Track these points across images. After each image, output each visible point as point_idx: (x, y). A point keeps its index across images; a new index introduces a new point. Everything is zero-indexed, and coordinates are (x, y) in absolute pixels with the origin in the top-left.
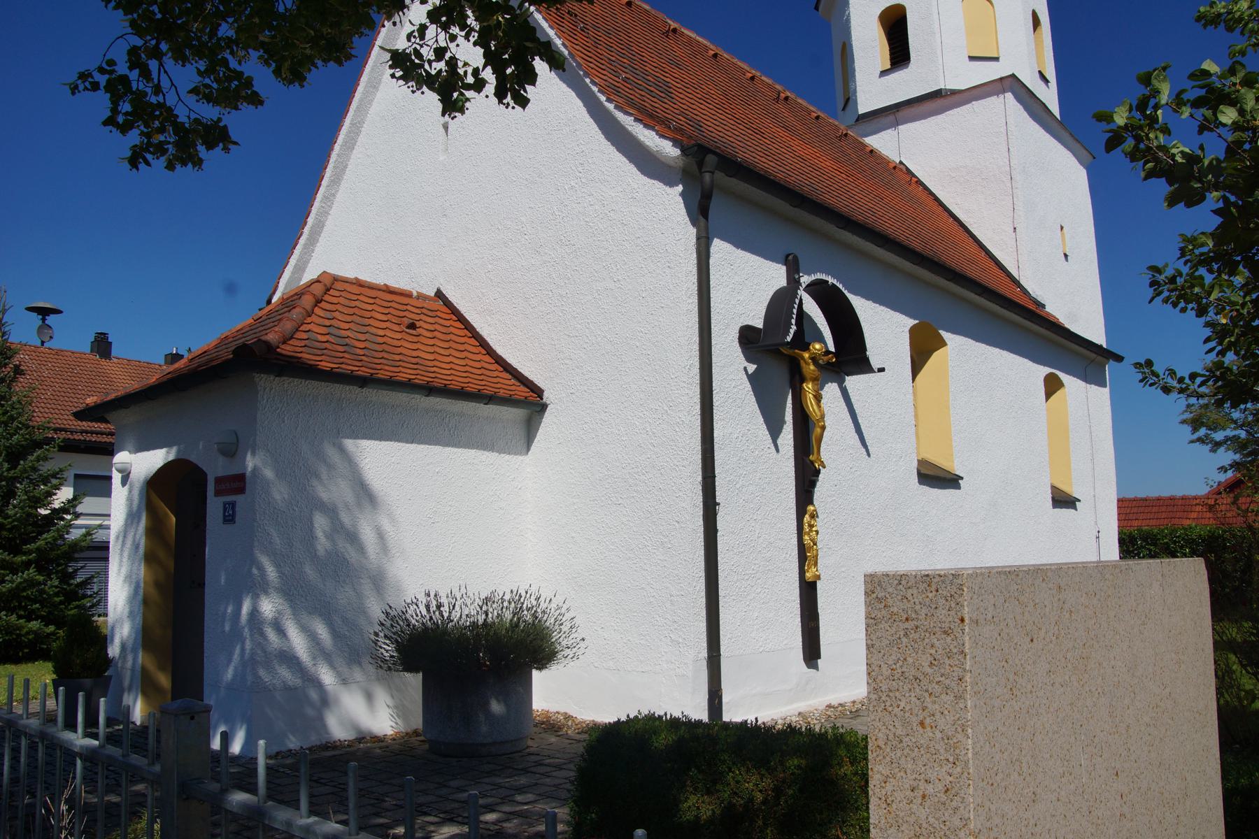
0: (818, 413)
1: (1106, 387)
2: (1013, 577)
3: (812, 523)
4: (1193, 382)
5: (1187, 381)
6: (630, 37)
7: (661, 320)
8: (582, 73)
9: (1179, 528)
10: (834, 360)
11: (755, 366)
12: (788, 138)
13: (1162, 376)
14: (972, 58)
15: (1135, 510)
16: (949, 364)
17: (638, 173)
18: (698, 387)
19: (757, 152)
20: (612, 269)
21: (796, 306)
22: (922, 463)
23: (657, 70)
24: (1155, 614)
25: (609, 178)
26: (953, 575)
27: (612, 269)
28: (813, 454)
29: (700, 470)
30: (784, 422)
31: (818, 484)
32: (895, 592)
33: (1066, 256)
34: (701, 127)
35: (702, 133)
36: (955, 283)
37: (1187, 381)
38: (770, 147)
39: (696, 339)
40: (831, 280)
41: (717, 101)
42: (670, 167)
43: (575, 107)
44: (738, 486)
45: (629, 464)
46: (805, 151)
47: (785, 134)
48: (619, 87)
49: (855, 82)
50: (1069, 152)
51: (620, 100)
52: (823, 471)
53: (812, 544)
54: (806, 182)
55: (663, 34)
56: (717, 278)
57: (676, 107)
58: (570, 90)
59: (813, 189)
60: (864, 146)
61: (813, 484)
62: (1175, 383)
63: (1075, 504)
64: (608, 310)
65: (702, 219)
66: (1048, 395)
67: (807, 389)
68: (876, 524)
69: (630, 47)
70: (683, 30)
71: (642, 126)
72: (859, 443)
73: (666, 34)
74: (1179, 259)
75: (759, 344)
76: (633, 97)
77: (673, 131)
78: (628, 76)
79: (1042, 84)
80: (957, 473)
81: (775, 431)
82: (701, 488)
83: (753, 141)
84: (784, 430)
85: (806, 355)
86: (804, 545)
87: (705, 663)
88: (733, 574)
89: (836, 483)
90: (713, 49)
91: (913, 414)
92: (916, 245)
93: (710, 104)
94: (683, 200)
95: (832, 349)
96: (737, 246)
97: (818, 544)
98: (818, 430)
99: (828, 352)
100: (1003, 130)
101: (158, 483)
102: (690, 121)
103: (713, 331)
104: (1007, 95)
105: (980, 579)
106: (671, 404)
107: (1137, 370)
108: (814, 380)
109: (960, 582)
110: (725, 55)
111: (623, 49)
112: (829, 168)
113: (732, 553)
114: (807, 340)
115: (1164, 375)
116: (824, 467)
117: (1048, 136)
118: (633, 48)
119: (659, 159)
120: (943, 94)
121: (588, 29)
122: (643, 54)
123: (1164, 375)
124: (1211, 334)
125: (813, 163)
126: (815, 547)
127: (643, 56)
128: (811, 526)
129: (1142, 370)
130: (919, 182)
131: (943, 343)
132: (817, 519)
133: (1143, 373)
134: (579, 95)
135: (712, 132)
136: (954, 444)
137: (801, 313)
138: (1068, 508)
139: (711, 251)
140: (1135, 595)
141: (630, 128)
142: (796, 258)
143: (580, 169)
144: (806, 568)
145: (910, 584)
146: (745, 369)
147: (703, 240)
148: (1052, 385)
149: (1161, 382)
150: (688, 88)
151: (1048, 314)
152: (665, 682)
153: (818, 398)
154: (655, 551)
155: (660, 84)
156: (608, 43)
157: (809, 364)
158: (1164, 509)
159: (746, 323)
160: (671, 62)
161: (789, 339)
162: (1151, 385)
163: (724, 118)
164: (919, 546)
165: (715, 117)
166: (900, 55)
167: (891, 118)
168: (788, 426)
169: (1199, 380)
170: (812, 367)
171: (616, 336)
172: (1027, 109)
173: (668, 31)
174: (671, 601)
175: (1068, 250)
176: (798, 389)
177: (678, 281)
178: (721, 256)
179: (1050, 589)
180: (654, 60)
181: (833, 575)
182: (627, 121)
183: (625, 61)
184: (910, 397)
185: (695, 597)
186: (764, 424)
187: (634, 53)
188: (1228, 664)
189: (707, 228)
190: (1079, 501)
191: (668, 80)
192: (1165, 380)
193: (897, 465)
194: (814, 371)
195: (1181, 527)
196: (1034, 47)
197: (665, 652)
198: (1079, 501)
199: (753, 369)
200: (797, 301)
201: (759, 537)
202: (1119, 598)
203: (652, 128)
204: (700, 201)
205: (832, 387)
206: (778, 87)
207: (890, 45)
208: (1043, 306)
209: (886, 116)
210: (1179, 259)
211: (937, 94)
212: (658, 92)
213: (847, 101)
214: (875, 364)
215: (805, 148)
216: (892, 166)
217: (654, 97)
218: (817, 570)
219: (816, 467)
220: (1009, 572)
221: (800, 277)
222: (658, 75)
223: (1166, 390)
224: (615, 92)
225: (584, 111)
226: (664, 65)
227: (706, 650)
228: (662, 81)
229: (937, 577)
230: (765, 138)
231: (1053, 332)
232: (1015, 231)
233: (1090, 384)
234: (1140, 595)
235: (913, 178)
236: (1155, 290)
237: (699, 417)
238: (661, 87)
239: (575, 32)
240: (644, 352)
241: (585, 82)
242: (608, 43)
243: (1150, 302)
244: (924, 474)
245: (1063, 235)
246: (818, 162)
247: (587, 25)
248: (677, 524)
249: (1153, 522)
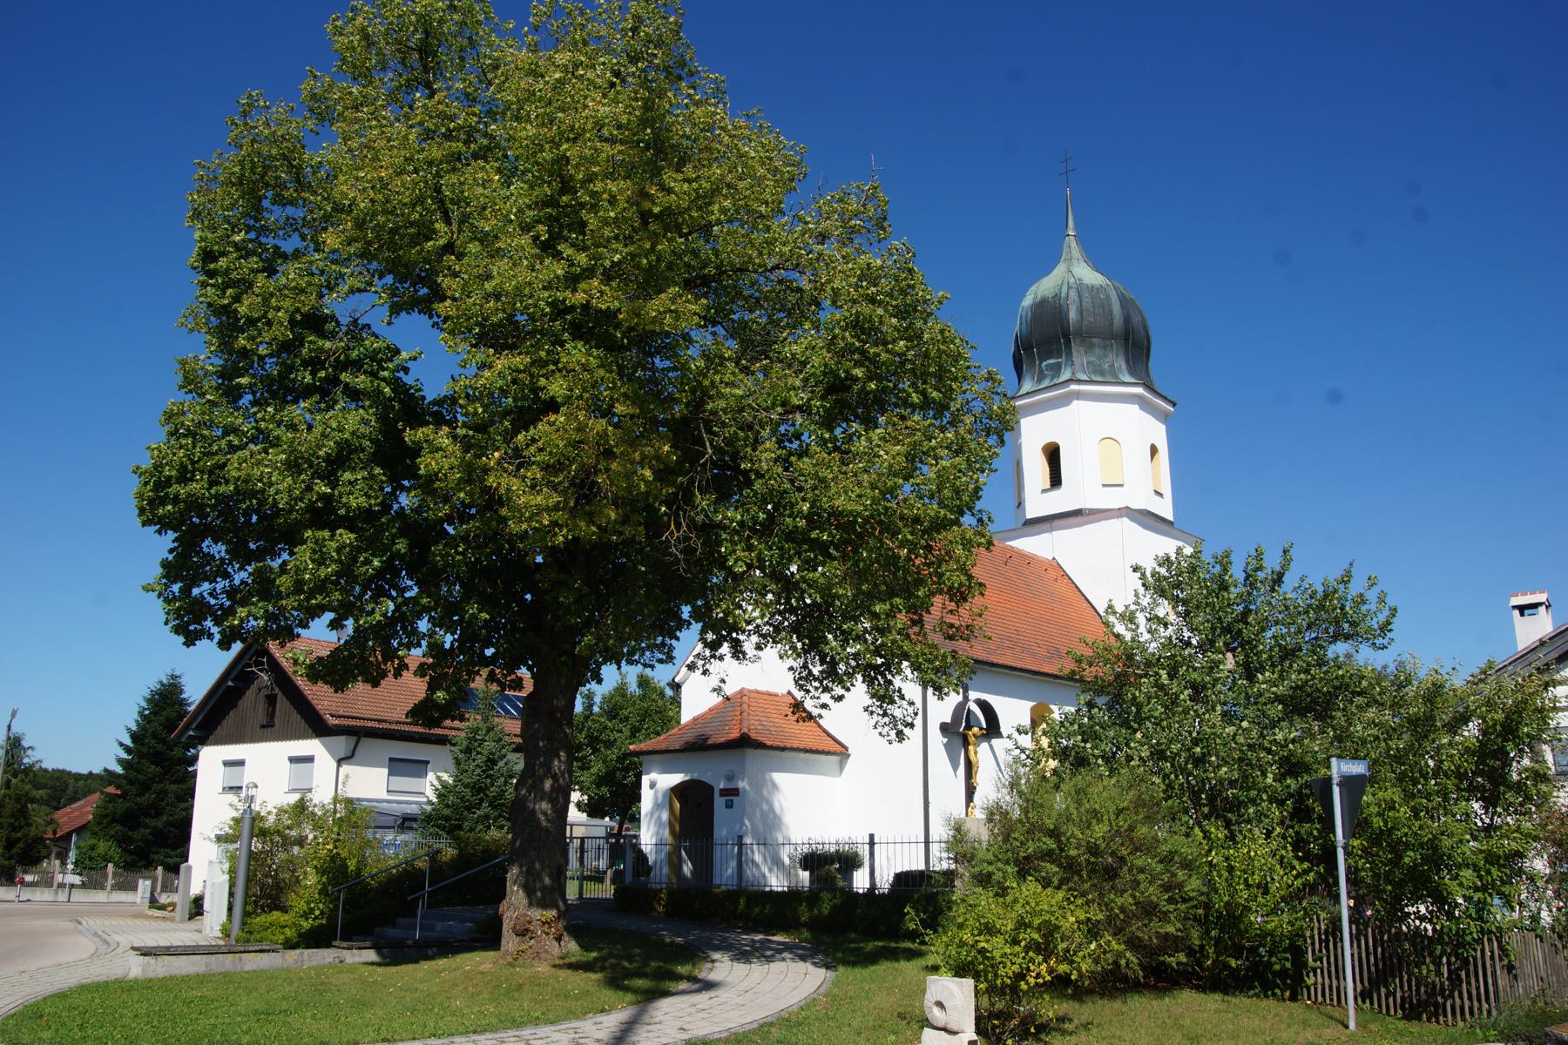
14: (1104, 485)
81: (955, 767)
101: (678, 791)
153: (976, 753)
166: (1056, 480)
167: (1047, 526)
211: (1077, 513)
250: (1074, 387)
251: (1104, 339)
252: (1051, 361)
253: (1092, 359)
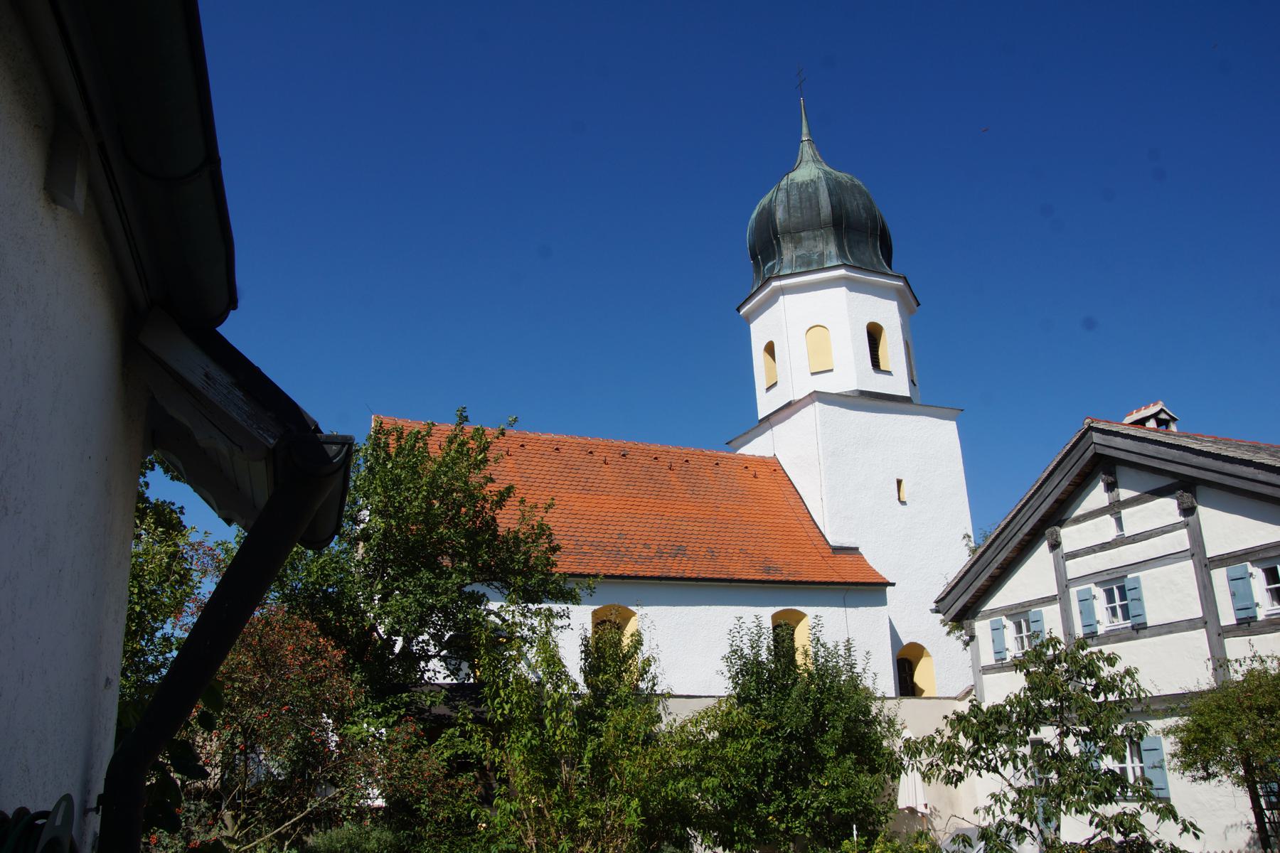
14: (813, 374)
211: (789, 404)
250: (775, 284)
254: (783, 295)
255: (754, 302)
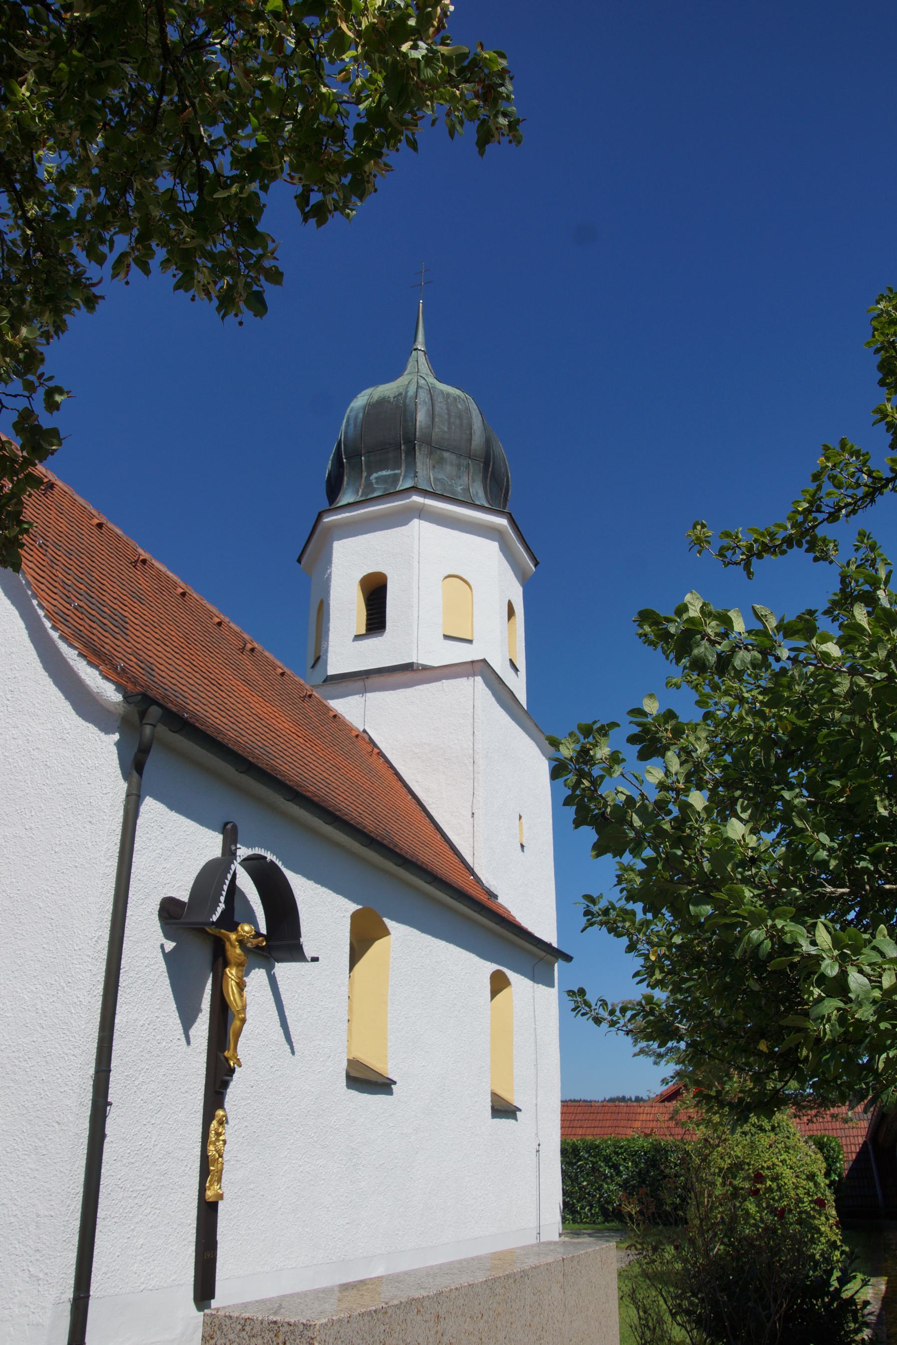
0: (239, 1004)
1: (552, 986)
2: (380, 1316)
3: (220, 1130)
4: (624, 1016)
5: (618, 1013)
6: (93, 562)
7: (72, 880)
8: (30, 593)
9: (622, 1139)
10: (264, 943)
11: (174, 944)
12: (247, 694)
13: (594, 1007)
14: (446, 637)
15: (580, 1117)
16: (392, 955)
17: (73, 712)
18: (105, 963)
19: (210, 705)
20: (26, 814)
21: (227, 882)
22: (353, 1063)
23: (116, 601)
24: (554, 1323)
25: (39, 712)
26: (304, 1325)
27: (26, 814)
28: (229, 1050)
29: (94, 1061)
30: (199, 1010)
31: (232, 1085)
32: (237, 1340)
33: (522, 846)
34: (153, 670)
35: (152, 678)
36: (404, 869)
37: (618, 1013)
38: (226, 701)
39: (110, 907)
40: (270, 856)
41: (175, 644)
42: (109, 711)
43: (16, 628)
44: (136, 1083)
45: (10, 1046)
46: (263, 710)
47: (245, 688)
48: (68, 616)
49: (328, 642)
50: (532, 741)
51: (67, 630)
52: (237, 1069)
53: (217, 1156)
54: (259, 743)
55: (131, 563)
56: (143, 841)
57: (129, 644)
58: (14, 608)
59: (265, 753)
60: (329, 709)
61: (225, 1085)
62: (605, 1014)
63: (516, 1114)
64: (14, 860)
65: (135, 775)
66: (494, 993)
67: (230, 975)
68: (294, 1133)
69: (91, 572)
70: (153, 562)
71: (85, 663)
72: (284, 1039)
73: (134, 564)
74: (615, 885)
75: (182, 920)
76: (82, 628)
77: (118, 674)
78: (81, 604)
79: (512, 671)
80: (390, 1077)
81: (188, 1019)
82: (92, 1083)
83: (208, 693)
84: (198, 1020)
85: (233, 937)
86: (208, 1157)
87: (68, 1307)
88: (119, 1190)
89: (252, 1084)
90: (182, 586)
91: (347, 1008)
92: (368, 824)
93: (167, 646)
94: (118, 750)
95: (263, 930)
96: (171, 807)
97: (224, 1156)
98: (237, 1023)
99: (258, 934)
100: (470, 712)
102: (142, 662)
103: (130, 900)
104: (476, 678)
105: (336, 1327)
106: (70, 981)
107: (570, 998)
108: (239, 965)
109: (311, 1335)
110: (195, 595)
111: (82, 574)
112: (287, 731)
113: (120, 1164)
114: (236, 919)
115: (596, 1005)
116: (240, 1066)
117: (513, 723)
118: (94, 574)
119: (97, 701)
120: (415, 668)
121: (48, 547)
122: (104, 582)
123: (596, 1005)
124: (641, 968)
125: (270, 723)
126: (220, 1159)
127: (104, 585)
128: (218, 1134)
129: (575, 999)
130: (381, 754)
131: (386, 932)
132: (226, 1125)
133: (576, 1002)
134: (22, 616)
135: (164, 678)
136: (389, 1044)
137: (233, 888)
138: (508, 1118)
139: (141, 810)
140: (531, 1306)
141: (72, 663)
142: (235, 828)
143: (9, 696)
144: (207, 1185)
145: (255, 1331)
146: (162, 946)
147: (133, 798)
148: (499, 984)
149: (593, 1013)
150: (147, 626)
151: (501, 906)
152: (13, 1333)
153: (241, 986)
154: (26, 1157)
155: (116, 618)
156: (67, 564)
157: (233, 946)
158: (608, 1116)
159: (169, 895)
160: (133, 594)
161: (215, 918)
162: (583, 1014)
163: (180, 663)
164: (341, 1160)
165: (170, 662)
167: (360, 684)
168: (204, 1015)
169: (629, 1014)
170: (238, 951)
171: (18, 892)
172: (495, 694)
173: (136, 561)
174: (37, 1223)
175: (524, 841)
176: (220, 975)
177: (98, 840)
178: (152, 816)
179: (426, 1321)
180: (115, 590)
181: (239, 1194)
182: (70, 654)
183: (82, 586)
184: (345, 990)
185: (67, 1219)
186: (176, 1011)
187: (93, 579)
188: (659, 1311)
189: (139, 785)
190: (520, 1110)
191: (126, 614)
192: (596, 1011)
193: (324, 1066)
194: (240, 955)
195: (624, 1137)
196: (507, 635)
197: (19, 1291)
198: (520, 1110)
199: (172, 947)
200: (229, 877)
201: (155, 1145)
202: (511, 1313)
203: (96, 667)
204: (136, 755)
205: (259, 974)
206: (246, 636)
207: (367, 610)
208: (496, 897)
209: (355, 681)
210: (615, 885)
211: (408, 667)
212: (112, 627)
213: (318, 659)
214: (309, 952)
215: (264, 706)
216: (354, 734)
217: (106, 631)
218: (220, 1188)
219: (230, 1065)
220: (375, 1311)
221: (237, 849)
222: (116, 607)
223: (598, 1021)
224: (62, 620)
225: (25, 633)
226: (125, 598)
227: (73, 1289)
228: (118, 614)
229: (285, 1325)
230: (222, 691)
231: (502, 927)
232: (473, 817)
233: (538, 983)
234: (537, 1304)
235: (375, 749)
236: (588, 920)
237: (101, 998)
238: (116, 621)
239: (32, 548)
240: (47, 915)
241: (32, 603)
242: (67, 564)
243: (583, 931)
244: (354, 1077)
245: (521, 824)
246: (276, 723)
247: (48, 541)
248: (56, 1125)
249: (597, 1131)
250: (417, 499)
251: (460, 456)
252: (384, 473)
253: (440, 476)
254: (420, 518)
255: (362, 511)
